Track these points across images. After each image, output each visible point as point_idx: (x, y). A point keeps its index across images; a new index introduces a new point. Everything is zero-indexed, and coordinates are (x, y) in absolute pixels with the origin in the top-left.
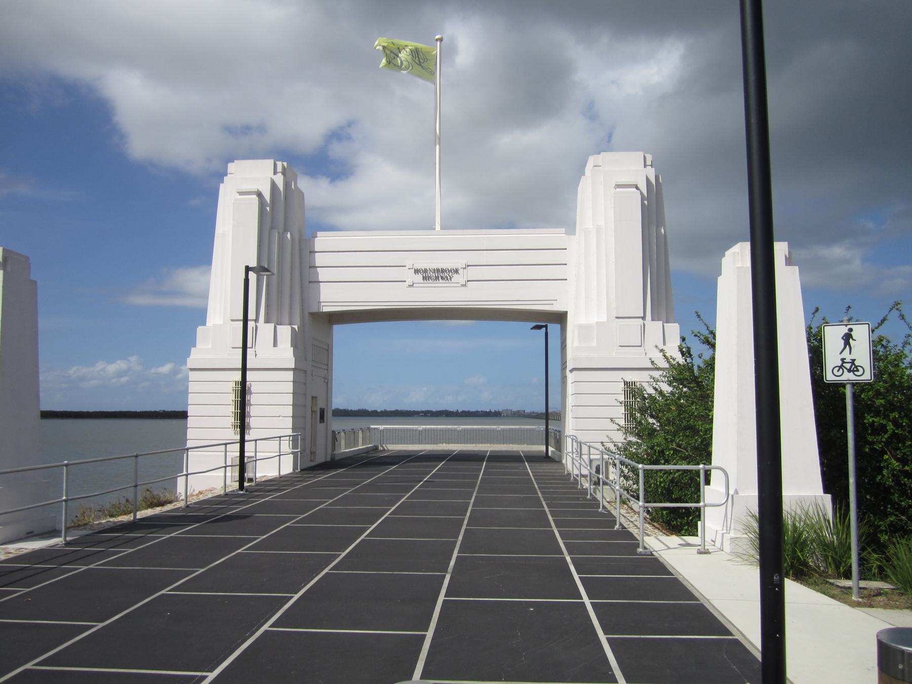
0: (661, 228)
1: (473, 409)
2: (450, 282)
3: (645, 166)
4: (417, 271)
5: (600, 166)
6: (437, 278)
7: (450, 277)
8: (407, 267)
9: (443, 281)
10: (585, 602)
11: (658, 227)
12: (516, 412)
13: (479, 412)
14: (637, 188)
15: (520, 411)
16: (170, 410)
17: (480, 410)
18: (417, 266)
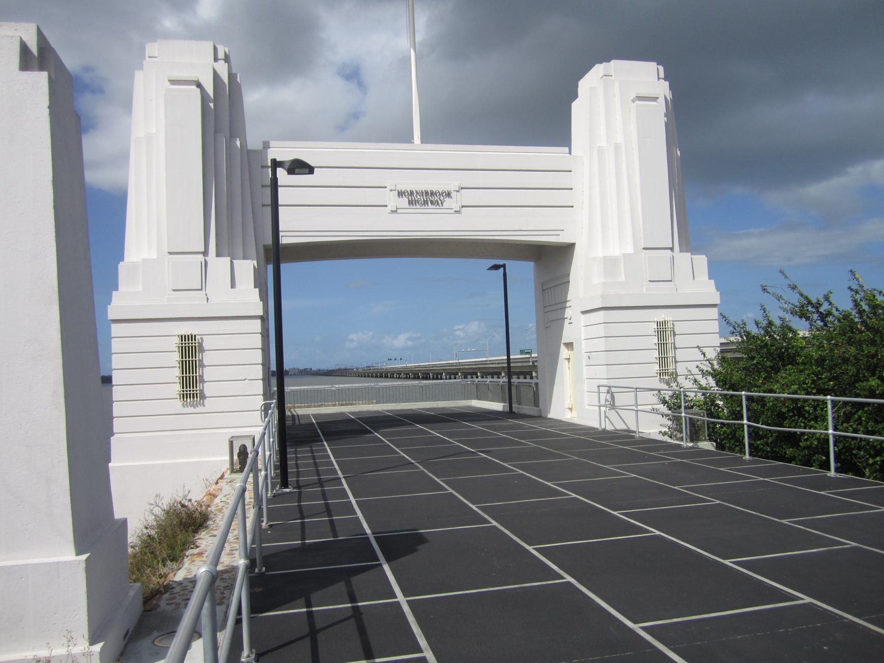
0: (236, 140)
2: (441, 207)
3: (659, 79)
4: (401, 194)
5: (156, 57)
6: (426, 203)
7: (441, 201)
8: (389, 188)
9: (433, 207)
10: (403, 598)
11: (232, 136)
14: (199, 85)
15: (307, 369)
18: (402, 188)
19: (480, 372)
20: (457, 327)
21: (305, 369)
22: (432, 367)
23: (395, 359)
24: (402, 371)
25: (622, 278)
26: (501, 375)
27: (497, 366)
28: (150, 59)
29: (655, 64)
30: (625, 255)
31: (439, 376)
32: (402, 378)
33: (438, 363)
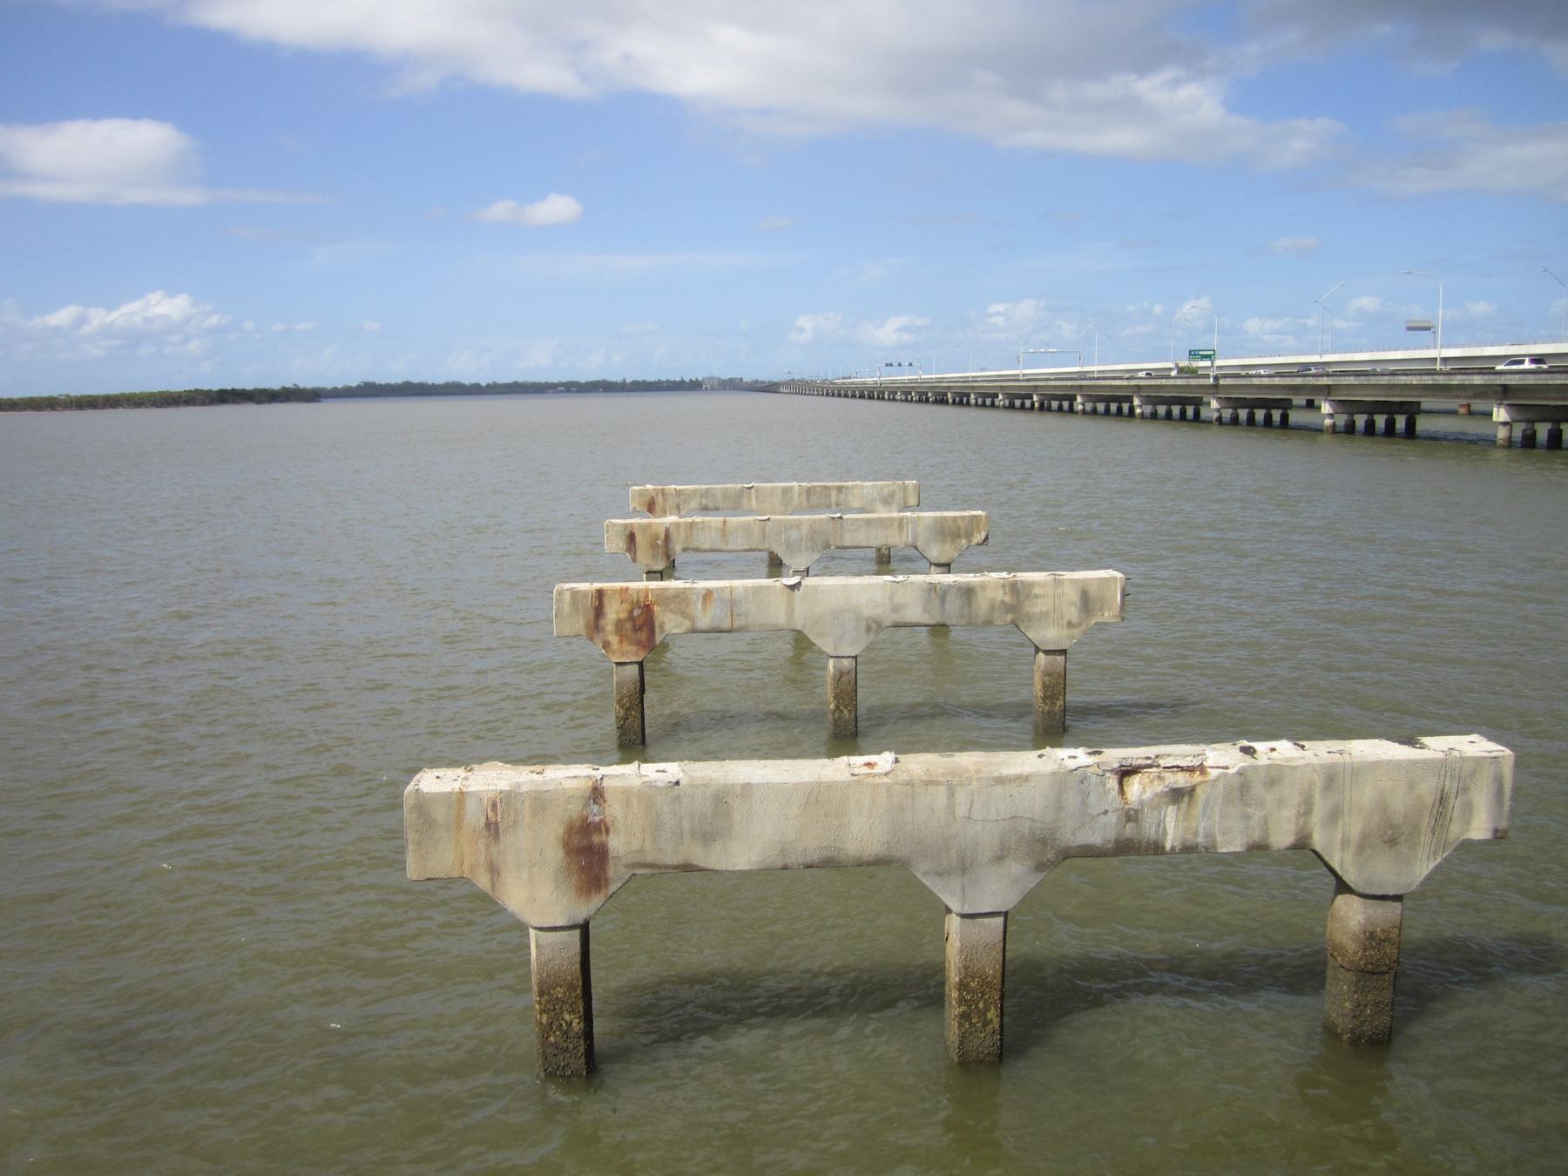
1: (651, 378)
12: (726, 381)
13: (663, 382)
15: (734, 379)
16: (156, 391)
17: (663, 379)
20: (995, 308)
22: (972, 381)
23: (900, 365)
24: (913, 387)
26: (1076, 400)
27: (1125, 383)
28: (620, 668)
32: (897, 400)
33: (979, 374)
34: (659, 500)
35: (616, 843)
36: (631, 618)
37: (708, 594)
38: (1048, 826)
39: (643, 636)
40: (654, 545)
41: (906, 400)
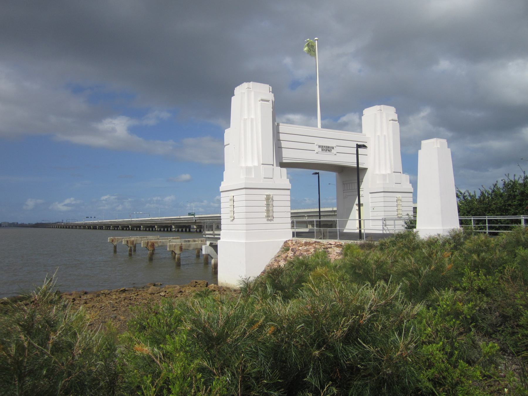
3: (270, 92)
4: (319, 147)
6: (326, 151)
12: (11, 223)
19: (157, 226)
21: (13, 223)
23: (91, 217)
25: (388, 182)
27: (170, 222)
29: (268, 85)
30: (389, 174)
31: (108, 228)
34: (114, 240)
35: (183, 248)
36: (151, 245)
37: (160, 242)
38: (62, 386)
39: (153, 247)
40: (131, 243)
41: (80, 228)
